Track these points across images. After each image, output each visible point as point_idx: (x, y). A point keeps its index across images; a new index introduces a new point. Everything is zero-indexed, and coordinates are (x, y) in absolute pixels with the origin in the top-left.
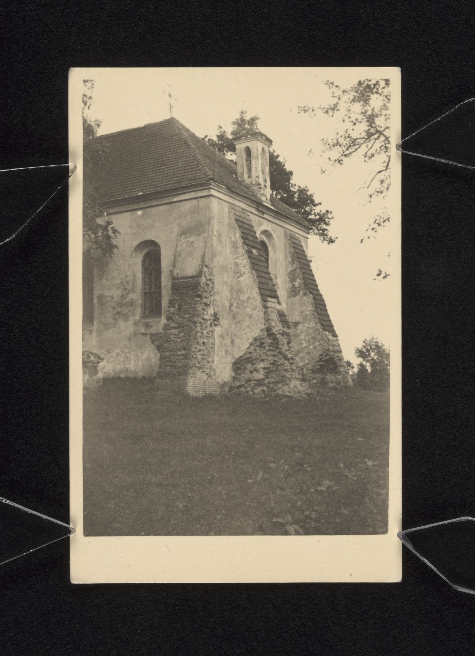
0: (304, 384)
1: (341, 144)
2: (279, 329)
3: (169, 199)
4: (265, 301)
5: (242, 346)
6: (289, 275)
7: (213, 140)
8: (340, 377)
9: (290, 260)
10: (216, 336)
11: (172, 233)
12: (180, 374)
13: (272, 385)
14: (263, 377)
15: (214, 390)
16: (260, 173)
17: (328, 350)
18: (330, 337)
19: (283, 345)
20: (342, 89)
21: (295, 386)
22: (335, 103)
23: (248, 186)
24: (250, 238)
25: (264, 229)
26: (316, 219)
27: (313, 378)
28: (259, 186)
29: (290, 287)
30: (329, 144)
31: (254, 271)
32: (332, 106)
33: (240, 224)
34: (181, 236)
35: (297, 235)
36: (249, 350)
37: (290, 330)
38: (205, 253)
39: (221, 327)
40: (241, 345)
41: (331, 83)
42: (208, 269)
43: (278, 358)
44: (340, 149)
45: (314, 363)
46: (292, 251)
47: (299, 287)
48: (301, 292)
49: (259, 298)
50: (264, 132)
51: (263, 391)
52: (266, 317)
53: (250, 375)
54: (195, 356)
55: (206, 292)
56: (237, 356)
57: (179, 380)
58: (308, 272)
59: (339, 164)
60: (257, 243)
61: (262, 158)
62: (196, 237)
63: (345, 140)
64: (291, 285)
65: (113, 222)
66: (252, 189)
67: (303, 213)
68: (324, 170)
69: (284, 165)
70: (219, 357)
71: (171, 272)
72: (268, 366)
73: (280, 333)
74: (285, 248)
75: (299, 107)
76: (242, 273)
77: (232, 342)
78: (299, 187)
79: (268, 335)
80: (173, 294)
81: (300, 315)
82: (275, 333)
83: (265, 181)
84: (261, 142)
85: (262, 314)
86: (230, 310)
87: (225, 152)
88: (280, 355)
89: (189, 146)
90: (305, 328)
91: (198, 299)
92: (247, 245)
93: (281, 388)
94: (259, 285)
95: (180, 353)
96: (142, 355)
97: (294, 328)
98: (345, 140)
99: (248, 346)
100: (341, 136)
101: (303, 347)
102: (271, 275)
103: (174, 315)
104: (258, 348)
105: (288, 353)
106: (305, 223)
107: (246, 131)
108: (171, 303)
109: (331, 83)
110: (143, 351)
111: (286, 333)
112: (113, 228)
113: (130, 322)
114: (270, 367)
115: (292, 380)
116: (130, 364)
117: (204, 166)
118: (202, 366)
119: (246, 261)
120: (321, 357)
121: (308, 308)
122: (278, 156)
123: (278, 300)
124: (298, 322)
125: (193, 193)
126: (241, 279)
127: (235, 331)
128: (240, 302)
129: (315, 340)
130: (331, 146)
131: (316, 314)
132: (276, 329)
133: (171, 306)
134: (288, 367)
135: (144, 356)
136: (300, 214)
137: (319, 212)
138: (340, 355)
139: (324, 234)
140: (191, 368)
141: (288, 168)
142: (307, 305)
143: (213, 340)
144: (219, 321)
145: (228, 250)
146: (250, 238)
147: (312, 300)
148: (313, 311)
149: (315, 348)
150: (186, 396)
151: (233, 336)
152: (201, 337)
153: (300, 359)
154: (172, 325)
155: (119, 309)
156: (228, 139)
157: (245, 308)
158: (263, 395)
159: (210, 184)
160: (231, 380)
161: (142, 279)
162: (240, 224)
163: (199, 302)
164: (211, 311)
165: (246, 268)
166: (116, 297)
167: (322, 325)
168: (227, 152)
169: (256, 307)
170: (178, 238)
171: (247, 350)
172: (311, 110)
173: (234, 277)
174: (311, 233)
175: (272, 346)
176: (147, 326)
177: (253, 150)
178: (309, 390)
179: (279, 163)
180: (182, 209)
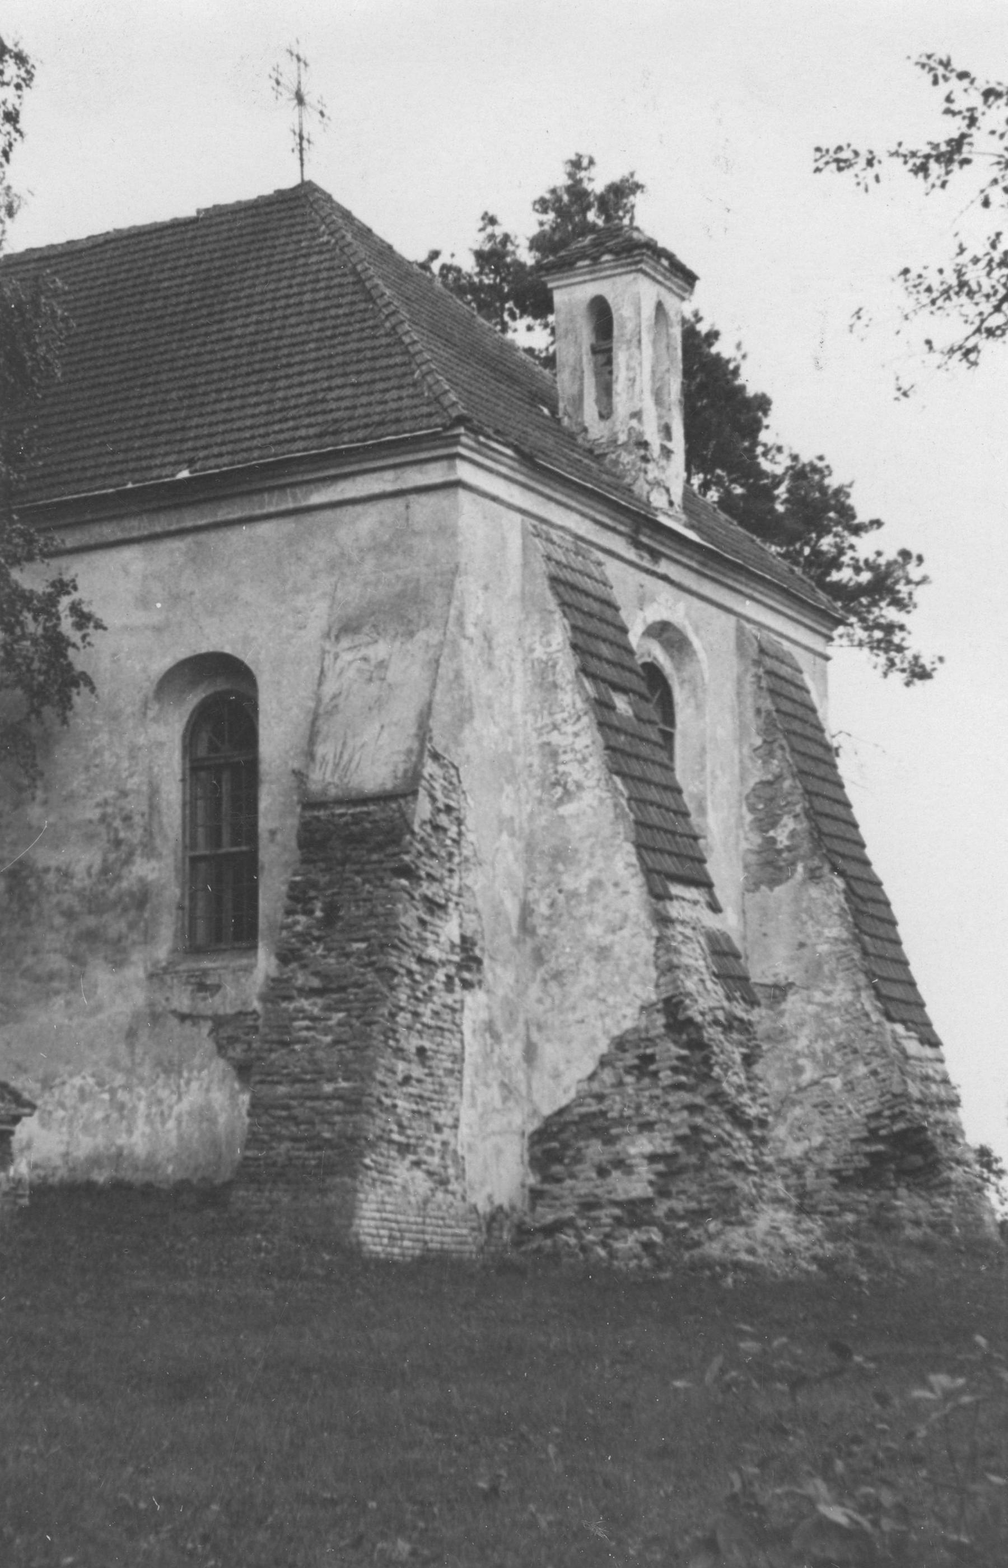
0: (807, 1224)
1: (975, 287)
2: (712, 1004)
3: (295, 498)
4: (658, 895)
5: (566, 1072)
6: (752, 800)
7: (458, 270)
8: (948, 1205)
9: (758, 741)
10: (467, 1029)
11: (302, 627)
12: (329, 1169)
13: (682, 1225)
14: (650, 1192)
15: (453, 1236)
16: (644, 400)
17: (905, 1096)
18: (913, 1047)
19: (726, 1068)
20: (982, 85)
21: (774, 1230)
22: (956, 135)
23: (597, 452)
24: (605, 650)
25: (658, 618)
26: (859, 585)
27: (840, 1204)
28: (642, 452)
29: (755, 848)
30: (929, 290)
31: (617, 780)
32: (944, 148)
33: (569, 596)
34: (337, 638)
35: (786, 645)
36: (596, 1086)
37: (756, 1011)
38: (429, 705)
39: (488, 992)
40: (562, 1067)
41: (941, 63)
42: (443, 766)
43: (708, 1120)
44: (971, 310)
45: (846, 1147)
46: (767, 704)
47: (789, 849)
48: (800, 868)
49: (635, 885)
50: (663, 242)
51: (648, 1246)
52: (663, 959)
53: (599, 1182)
54: (388, 1102)
55: (433, 855)
56: (547, 1110)
57: (324, 1192)
58: (828, 790)
59: (965, 364)
60: (631, 670)
61: (655, 342)
62: (398, 644)
63: (989, 274)
64: (759, 841)
65: (79, 582)
66: (616, 463)
67: (809, 563)
68: (905, 387)
69: (736, 372)
70: (480, 1109)
71: (300, 776)
72: (668, 1148)
73: (716, 1022)
74: (739, 694)
75: (818, 149)
76: (571, 787)
77: (530, 1054)
78: (795, 458)
79: (667, 1026)
80: (304, 861)
81: (792, 959)
82: (699, 1019)
83: (667, 431)
84: (654, 279)
85: (647, 947)
86: (526, 927)
87: (506, 317)
88: (715, 1108)
89: (374, 293)
90: (811, 1009)
91: (404, 882)
92: (593, 676)
93: (719, 1233)
94: (638, 834)
95: (328, 1088)
96: (180, 1099)
97: (770, 1007)
98: (989, 274)
99: (589, 1066)
100: (976, 260)
101: (803, 1094)
102: (685, 797)
103: (307, 943)
104: (629, 1079)
105: (745, 1098)
106: (817, 600)
107: (590, 237)
108: (298, 897)
109: (941, 63)
110: (182, 1082)
111: (741, 1021)
112: (75, 609)
113: (136, 971)
114: (675, 1155)
115: (760, 1205)
116: (130, 1132)
117: (430, 372)
118: (413, 1141)
119: (588, 742)
120: (873, 1124)
121: (827, 932)
122: (713, 336)
123: (712, 895)
124: (783, 983)
125: (389, 475)
126: (567, 809)
127: (541, 1008)
128: (561, 898)
129: (851, 1057)
130: (935, 294)
131: (857, 956)
132: (703, 1004)
133: (299, 906)
134: (747, 1155)
135: (185, 1105)
136: (797, 563)
137: (872, 557)
138: (949, 1115)
139: (890, 642)
140: (372, 1146)
141: (753, 381)
142: (823, 917)
143: (457, 1044)
144: (479, 970)
145: (519, 696)
146: (605, 650)
147: (842, 898)
148: (844, 942)
149: (850, 1086)
150: (351, 1253)
151: (533, 1030)
152: (409, 1028)
153: (791, 1133)
154: (300, 980)
155: (91, 921)
156: (521, 265)
157: (580, 921)
158: (646, 1262)
159: (455, 440)
160: (522, 1204)
161: (184, 805)
162: (567, 598)
163: (406, 896)
164: (450, 929)
165: (587, 766)
166: (79, 869)
167: (879, 996)
168: (513, 317)
169: (625, 918)
170: (328, 646)
171: (585, 1086)
172: (862, 162)
173: (540, 801)
174: (837, 642)
175: (686, 1073)
176: (202, 986)
177: (622, 312)
178: (829, 1246)
179: (718, 363)
180: (343, 534)
